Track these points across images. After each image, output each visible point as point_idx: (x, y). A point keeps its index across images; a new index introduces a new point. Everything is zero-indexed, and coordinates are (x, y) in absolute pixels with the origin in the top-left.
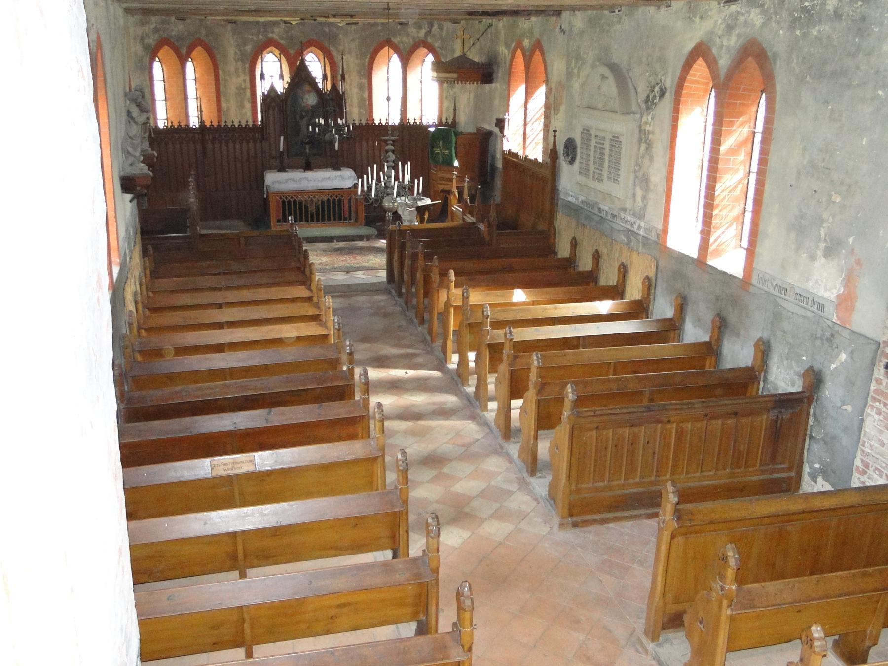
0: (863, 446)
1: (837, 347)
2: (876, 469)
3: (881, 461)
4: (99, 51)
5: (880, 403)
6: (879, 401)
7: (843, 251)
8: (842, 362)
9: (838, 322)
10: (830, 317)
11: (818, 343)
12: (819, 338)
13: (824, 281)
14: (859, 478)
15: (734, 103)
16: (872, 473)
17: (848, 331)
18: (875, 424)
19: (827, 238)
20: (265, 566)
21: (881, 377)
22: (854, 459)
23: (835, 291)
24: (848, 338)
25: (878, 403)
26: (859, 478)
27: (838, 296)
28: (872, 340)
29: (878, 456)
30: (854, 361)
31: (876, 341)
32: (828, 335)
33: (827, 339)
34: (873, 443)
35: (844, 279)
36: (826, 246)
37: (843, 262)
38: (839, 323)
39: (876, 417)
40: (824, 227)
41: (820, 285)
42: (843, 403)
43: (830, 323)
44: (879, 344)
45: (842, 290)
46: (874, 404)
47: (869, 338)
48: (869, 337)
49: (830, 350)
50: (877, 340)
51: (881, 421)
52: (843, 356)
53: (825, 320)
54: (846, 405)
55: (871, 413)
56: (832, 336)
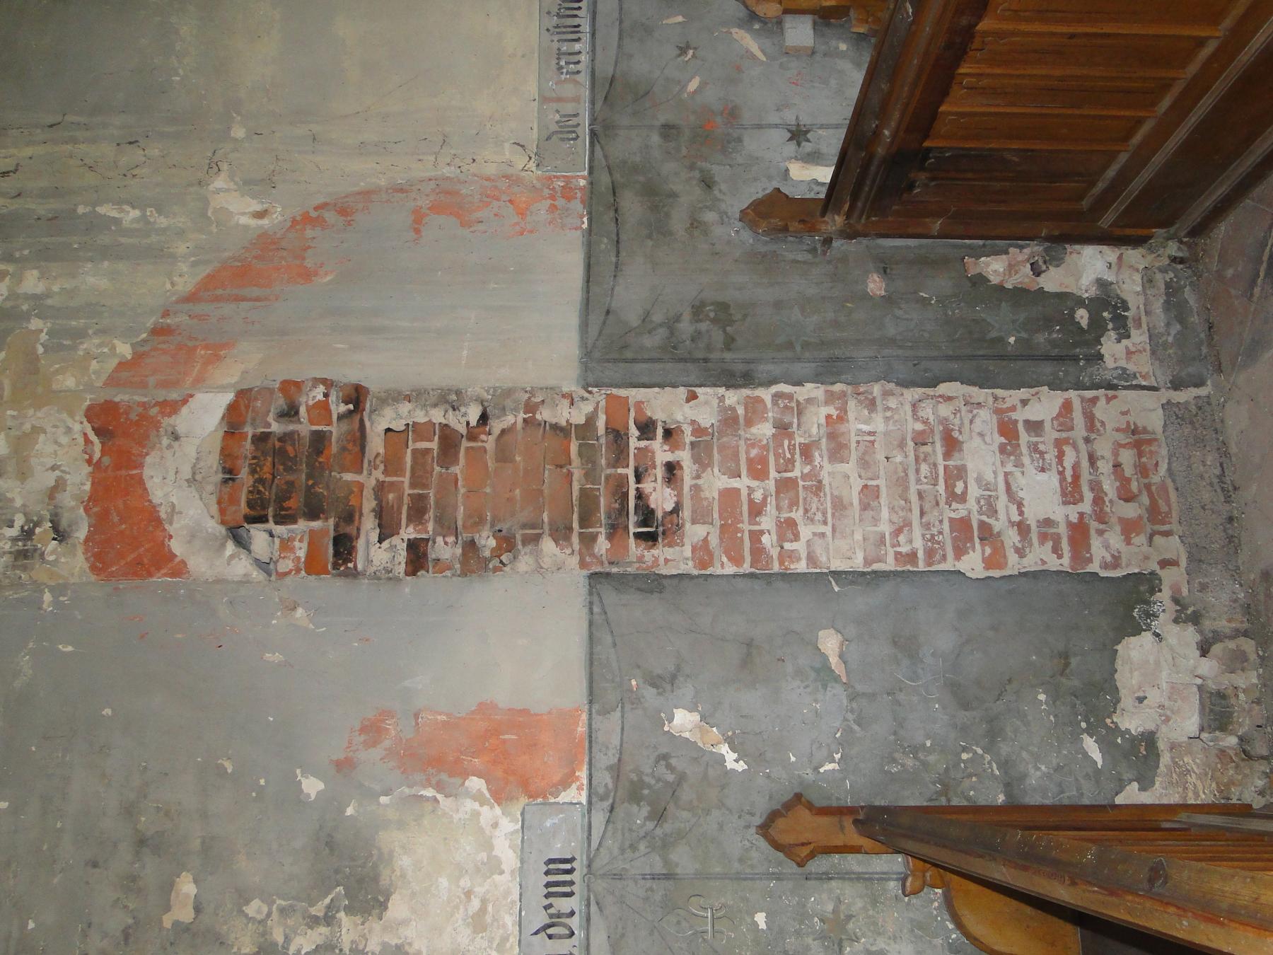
0: (912, 556)
1: (665, 757)
2: (953, 497)
3: (918, 481)
4: (594, 844)
5: (762, 532)
6: (756, 536)
7: (350, 811)
8: (703, 718)
9: (583, 774)
10: (577, 817)
11: (684, 861)
12: (666, 862)
13: (465, 882)
14: (1020, 553)
15: (480, 448)
16: (972, 503)
17: (598, 721)
18: (828, 530)
19: (318, 910)
20: (584, 326)
21: (688, 551)
22: (1113, 675)
23: (489, 813)
24: (618, 714)
25: (765, 539)
26: (1020, 553)
27: (499, 796)
28: (591, 612)
29: (914, 498)
30: (678, 668)
31: (591, 593)
32: (639, 815)
33: (659, 816)
34: (885, 528)
35: (439, 787)
36: (350, 910)
37: (384, 800)
38: (585, 767)
39: (805, 531)
40: (288, 939)
41: (484, 902)
42: (824, 673)
43: (599, 819)
44: (593, 576)
45: (476, 783)
46: (775, 556)
47: (591, 624)
48: (585, 625)
49: (686, 794)
50: (583, 589)
51: (806, 511)
52: (683, 721)
53: (594, 844)
54: (825, 658)
55: (804, 555)
56: (635, 795)
